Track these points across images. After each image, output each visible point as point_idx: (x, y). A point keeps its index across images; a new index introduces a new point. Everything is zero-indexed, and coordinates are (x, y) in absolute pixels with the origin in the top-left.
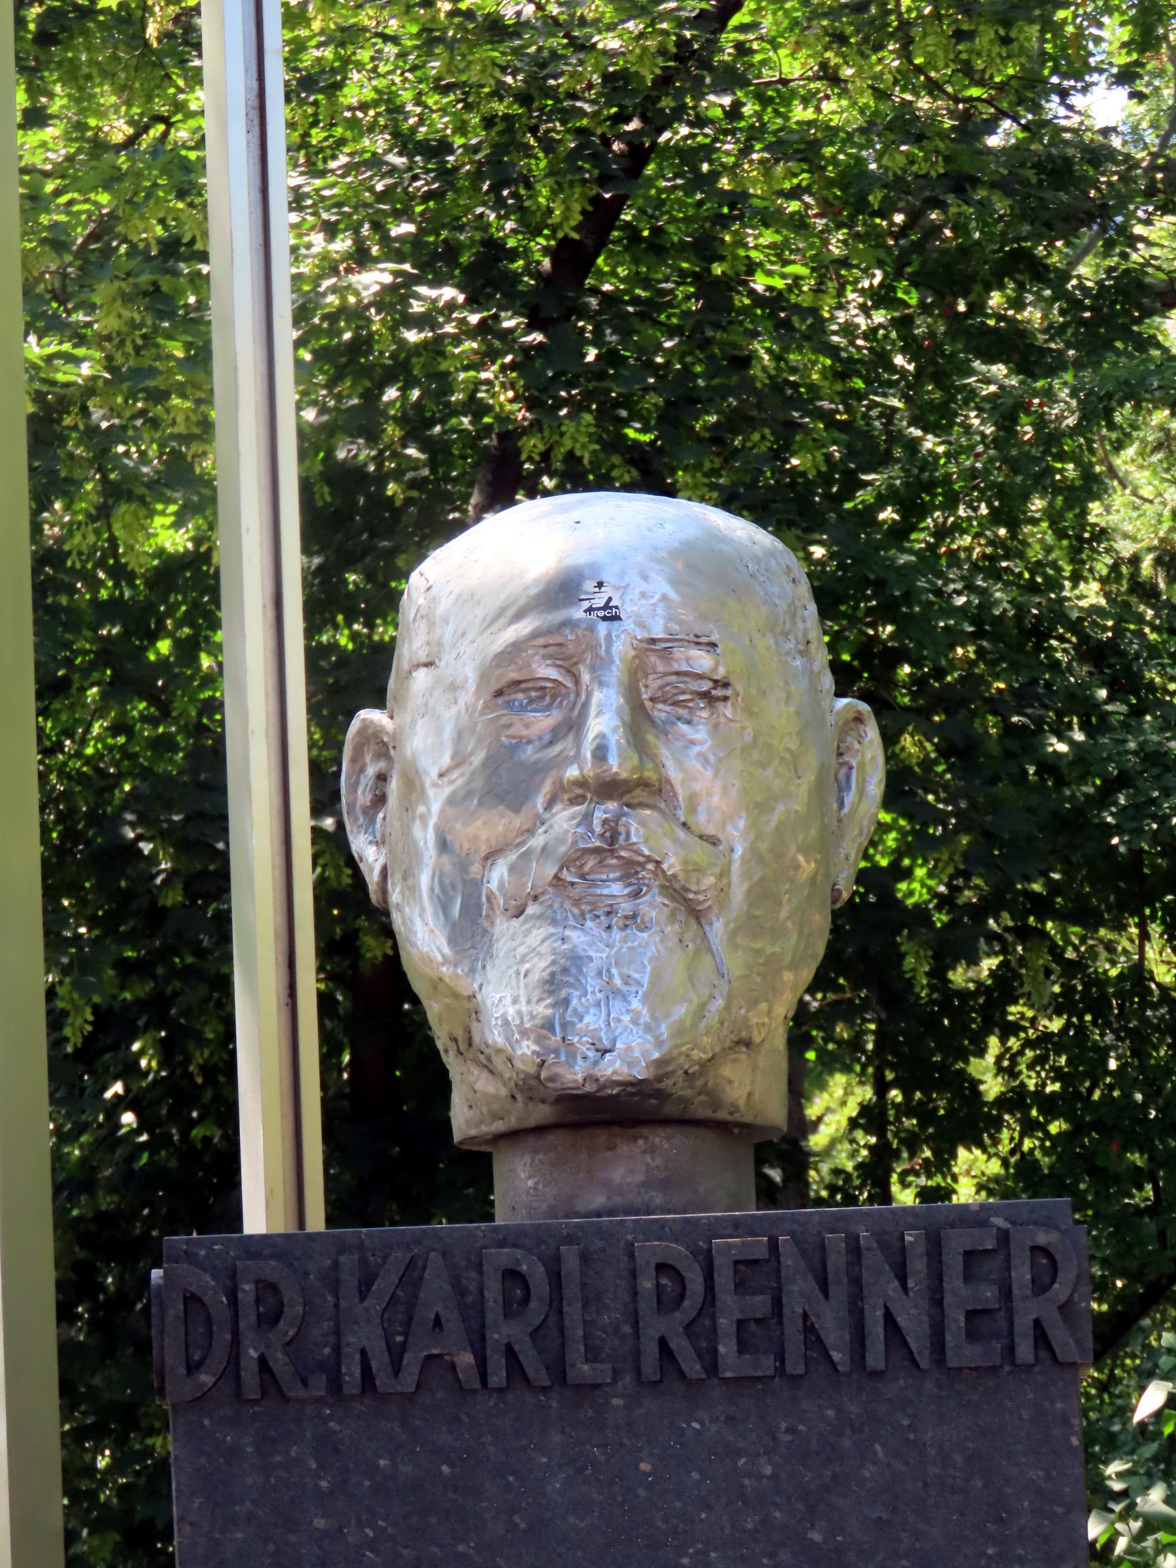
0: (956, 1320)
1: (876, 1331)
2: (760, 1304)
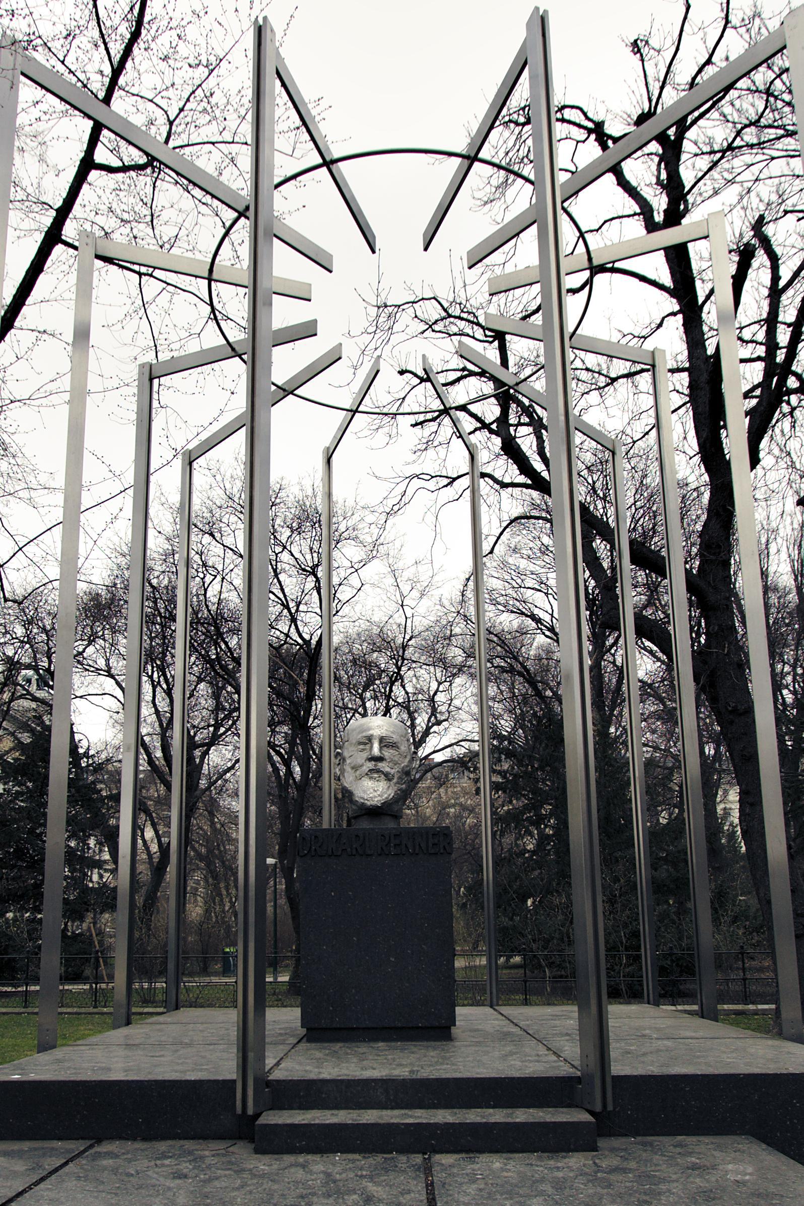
0: (430, 845)
1: (417, 847)
2: (397, 842)
